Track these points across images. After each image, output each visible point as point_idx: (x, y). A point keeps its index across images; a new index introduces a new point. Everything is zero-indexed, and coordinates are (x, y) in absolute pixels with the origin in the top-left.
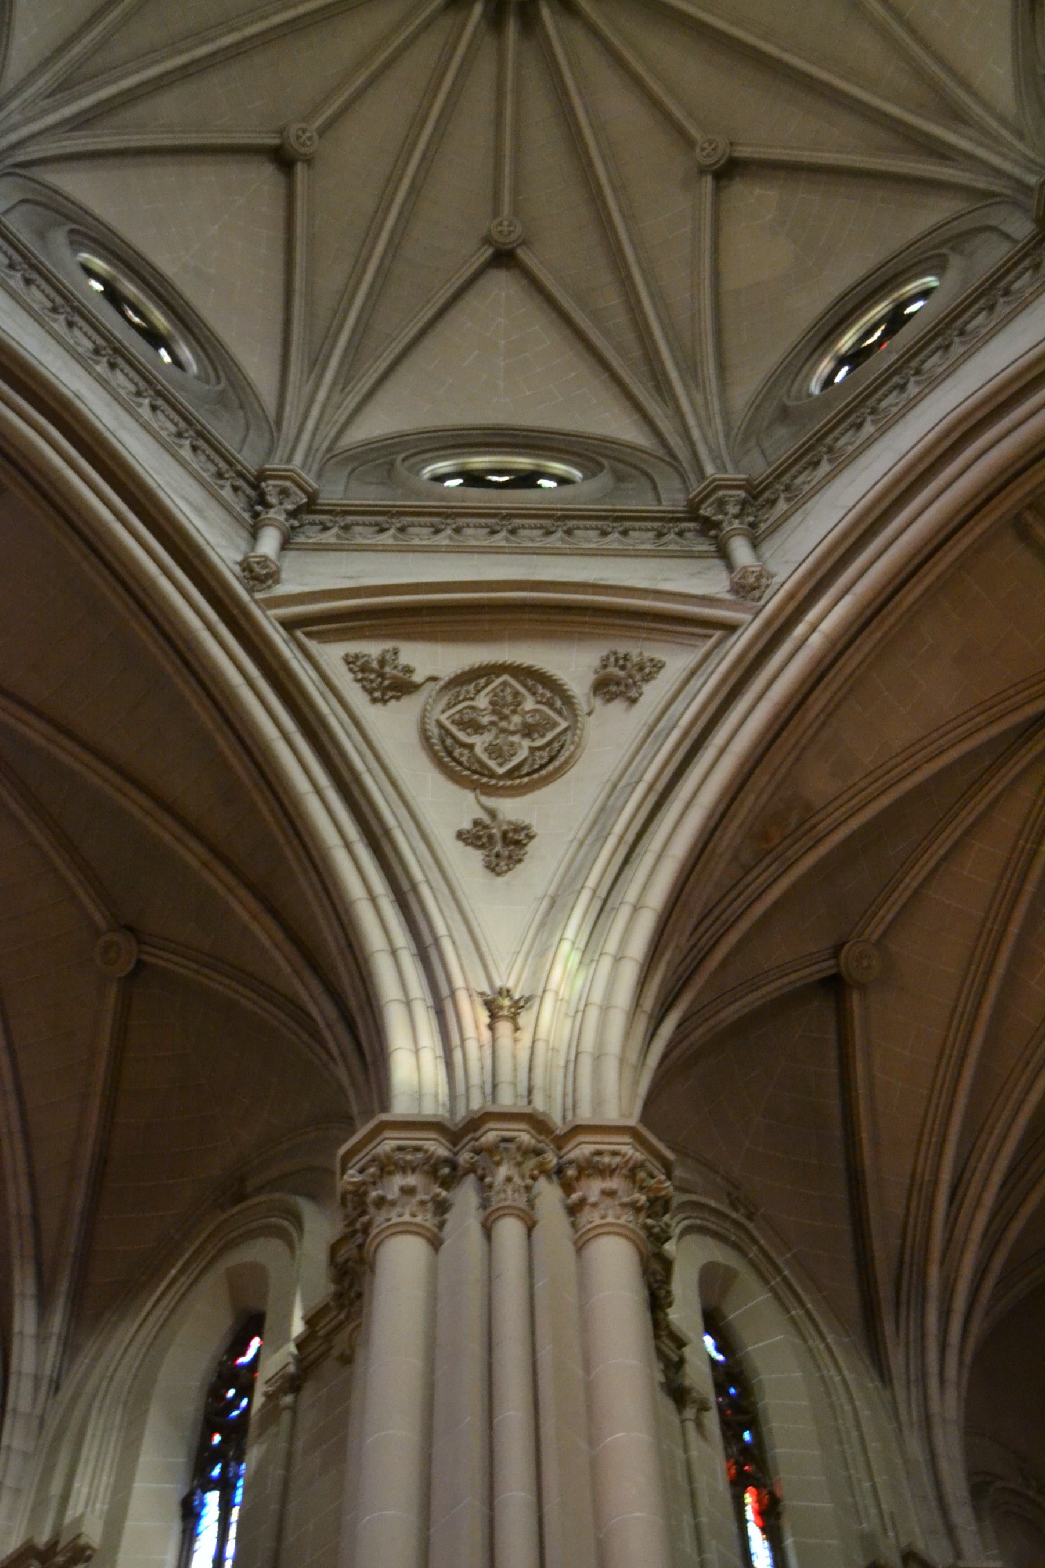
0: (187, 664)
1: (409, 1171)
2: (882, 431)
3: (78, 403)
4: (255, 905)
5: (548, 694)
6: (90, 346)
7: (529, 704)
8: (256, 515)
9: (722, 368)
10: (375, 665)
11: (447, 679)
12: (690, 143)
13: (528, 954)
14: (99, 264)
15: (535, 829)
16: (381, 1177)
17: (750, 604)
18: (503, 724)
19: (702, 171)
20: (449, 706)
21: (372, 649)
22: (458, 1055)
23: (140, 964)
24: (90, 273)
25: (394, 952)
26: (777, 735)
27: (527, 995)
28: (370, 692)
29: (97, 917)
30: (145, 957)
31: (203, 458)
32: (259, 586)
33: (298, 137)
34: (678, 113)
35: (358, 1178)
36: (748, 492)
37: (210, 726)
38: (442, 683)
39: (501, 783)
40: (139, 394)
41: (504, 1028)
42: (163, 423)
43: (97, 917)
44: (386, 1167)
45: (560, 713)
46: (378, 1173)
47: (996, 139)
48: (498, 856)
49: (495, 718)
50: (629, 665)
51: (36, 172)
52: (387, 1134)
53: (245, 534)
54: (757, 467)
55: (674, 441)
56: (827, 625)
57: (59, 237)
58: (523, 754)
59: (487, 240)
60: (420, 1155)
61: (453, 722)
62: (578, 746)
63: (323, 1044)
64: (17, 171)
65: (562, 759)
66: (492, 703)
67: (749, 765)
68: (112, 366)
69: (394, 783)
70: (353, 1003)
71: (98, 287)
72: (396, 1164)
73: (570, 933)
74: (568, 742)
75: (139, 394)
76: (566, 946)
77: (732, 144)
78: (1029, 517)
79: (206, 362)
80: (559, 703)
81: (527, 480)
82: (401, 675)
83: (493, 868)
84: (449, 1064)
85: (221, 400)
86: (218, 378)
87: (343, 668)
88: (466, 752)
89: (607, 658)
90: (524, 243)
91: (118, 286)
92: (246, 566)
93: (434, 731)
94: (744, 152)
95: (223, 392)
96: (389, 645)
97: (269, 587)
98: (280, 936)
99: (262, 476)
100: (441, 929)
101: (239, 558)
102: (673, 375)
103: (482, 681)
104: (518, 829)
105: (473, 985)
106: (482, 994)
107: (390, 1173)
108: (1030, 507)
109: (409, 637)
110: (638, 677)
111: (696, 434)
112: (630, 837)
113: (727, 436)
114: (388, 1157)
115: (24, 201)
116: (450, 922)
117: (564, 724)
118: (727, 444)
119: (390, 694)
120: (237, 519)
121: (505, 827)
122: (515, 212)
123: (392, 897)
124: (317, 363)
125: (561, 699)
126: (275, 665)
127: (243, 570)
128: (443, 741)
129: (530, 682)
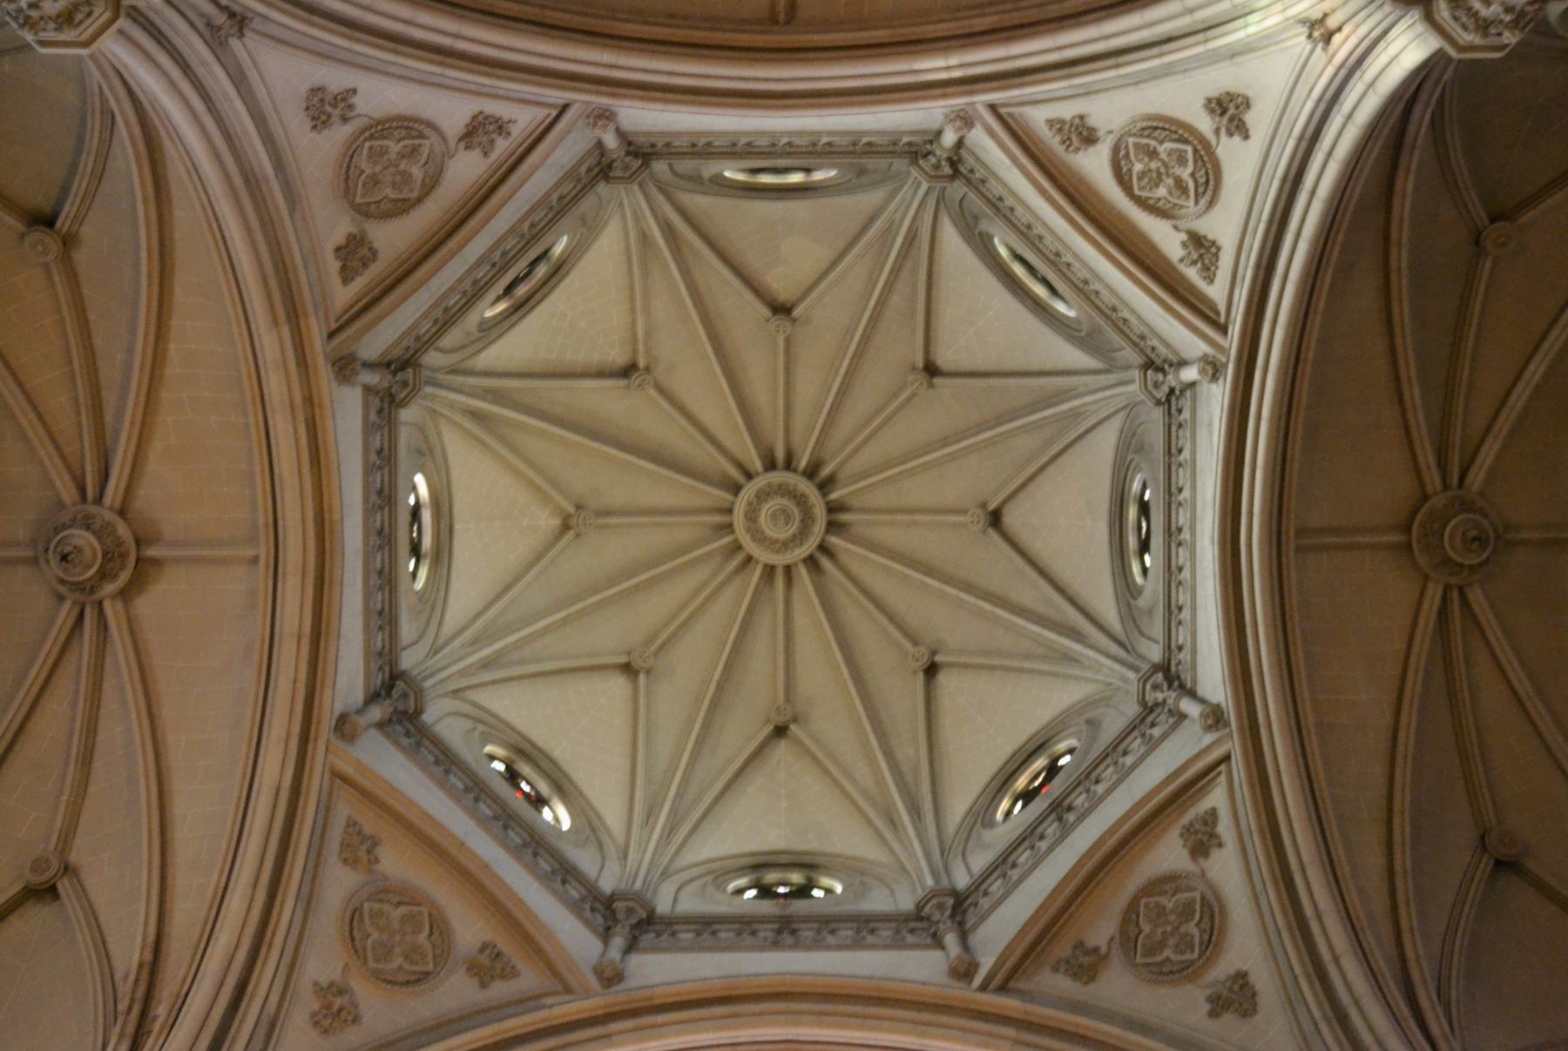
0: (1297, 360)
1: (1474, 11)
2: (819, 133)
3: (1216, 539)
4: (1397, 201)
5: (1123, 163)
6: (1181, 550)
7: (1138, 167)
8: (1182, 391)
9: (871, 220)
10: (1199, 265)
11: (1169, 222)
12: (788, 340)
13: (1277, 43)
14: (1136, 569)
15: (1202, 101)
16: (1493, 22)
17: (970, 112)
18: (1162, 170)
19: (794, 321)
20: (1182, 207)
21: (1192, 274)
22: (1375, 34)
23: (1493, 220)
24: (1145, 571)
25: (1349, 117)
26: (1022, 26)
27: (1300, 25)
28: (1216, 255)
29: (1488, 265)
30: (1486, 221)
31: (1181, 442)
32: (1218, 364)
33: (978, 522)
34: (781, 359)
35: (1507, 34)
36: (917, 161)
37: (1319, 317)
38: (1174, 222)
39: (1195, 142)
40: (1180, 465)
41: (1332, 23)
42: (1182, 477)
43: (1488, 265)
44: (1484, 26)
45: (1127, 147)
46: (1492, 26)
47: (635, 213)
48: (1237, 108)
49: (1164, 177)
50: (1065, 138)
51: (1123, 638)
52: (1461, 42)
53: (1198, 389)
54: (899, 164)
55: (930, 209)
56: (939, 62)
57: (1143, 602)
58: (1168, 145)
59: (931, 386)
60: (1457, 14)
61: (1188, 197)
62: (1135, 122)
63: (1442, 96)
64: (1129, 648)
65: (1149, 124)
66: (1157, 186)
67: (1053, 26)
68: (1180, 530)
69: (1253, 199)
70: (1401, 106)
71: (1147, 558)
72: (1477, 21)
73: (1241, 34)
74: (1138, 128)
75: (1180, 465)
76: (1251, 30)
77: (768, 321)
78: (782, 17)
79: (1130, 473)
80: (1122, 153)
81: (1052, 770)
82: (1191, 248)
83: (1247, 104)
84: (1386, 32)
85: (1141, 449)
86: (1131, 462)
87: (1218, 280)
88: (1198, 175)
89: (1073, 151)
90: (914, 368)
91: (1136, 548)
92: (1214, 378)
93: (1203, 202)
94: (765, 311)
95: (1136, 452)
96: (1182, 268)
97: (1214, 357)
98: (1401, 174)
99: (1159, 403)
100: (1310, 105)
101: (1214, 386)
102: (899, 240)
103: (1152, 202)
104: (1212, 111)
105: (1324, 60)
106: (1324, 49)
107: (1485, 20)
108: (776, 22)
109: (1167, 262)
110: (1067, 127)
111: (916, 204)
112: (1155, 51)
113: (902, 186)
114: (1476, 30)
115: (1142, 634)
116: (1301, 103)
117: (1131, 140)
118: (906, 183)
119: (1207, 244)
120: (1194, 400)
121: (1217, 119)
122: (902, 387)
123: (1318, 145)
124: (1076, 414)
125: (1118, 153)
126: (1252, 318)
127: (1218, 379)
128: (1204, 192)
129: (1126, 178)
